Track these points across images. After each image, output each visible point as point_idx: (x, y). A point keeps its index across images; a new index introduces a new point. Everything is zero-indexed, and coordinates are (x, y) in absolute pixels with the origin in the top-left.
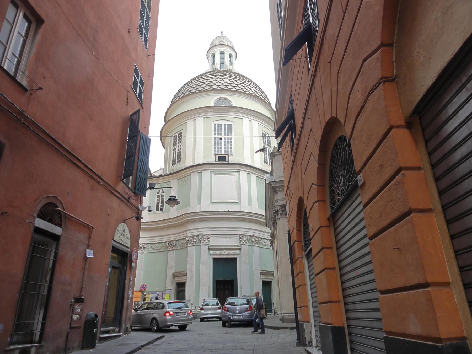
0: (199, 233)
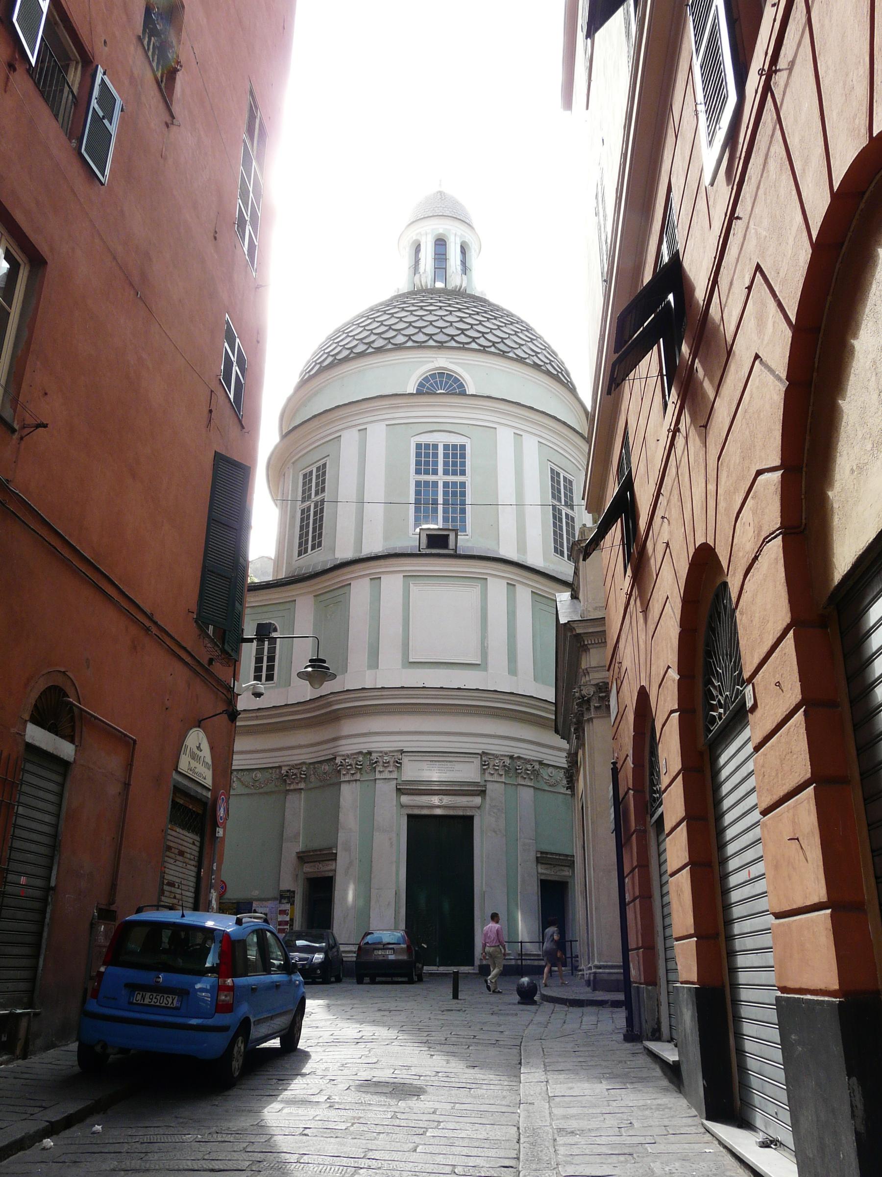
0: (373, 747)
